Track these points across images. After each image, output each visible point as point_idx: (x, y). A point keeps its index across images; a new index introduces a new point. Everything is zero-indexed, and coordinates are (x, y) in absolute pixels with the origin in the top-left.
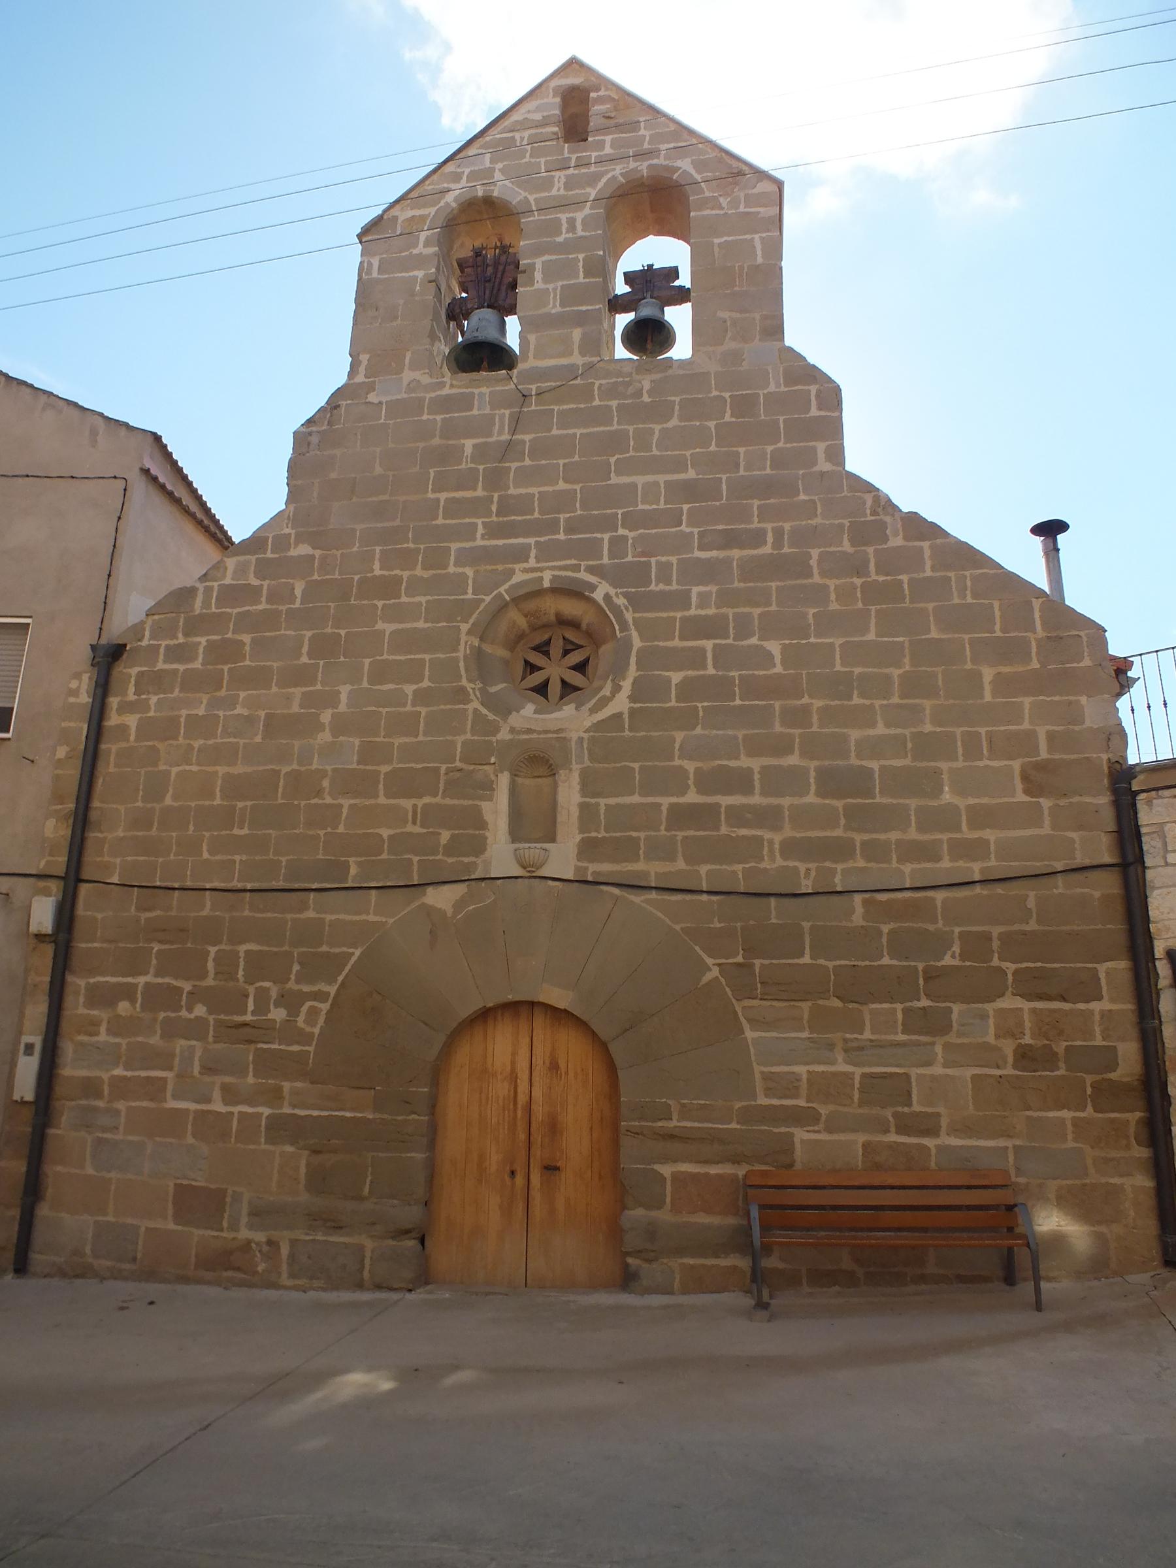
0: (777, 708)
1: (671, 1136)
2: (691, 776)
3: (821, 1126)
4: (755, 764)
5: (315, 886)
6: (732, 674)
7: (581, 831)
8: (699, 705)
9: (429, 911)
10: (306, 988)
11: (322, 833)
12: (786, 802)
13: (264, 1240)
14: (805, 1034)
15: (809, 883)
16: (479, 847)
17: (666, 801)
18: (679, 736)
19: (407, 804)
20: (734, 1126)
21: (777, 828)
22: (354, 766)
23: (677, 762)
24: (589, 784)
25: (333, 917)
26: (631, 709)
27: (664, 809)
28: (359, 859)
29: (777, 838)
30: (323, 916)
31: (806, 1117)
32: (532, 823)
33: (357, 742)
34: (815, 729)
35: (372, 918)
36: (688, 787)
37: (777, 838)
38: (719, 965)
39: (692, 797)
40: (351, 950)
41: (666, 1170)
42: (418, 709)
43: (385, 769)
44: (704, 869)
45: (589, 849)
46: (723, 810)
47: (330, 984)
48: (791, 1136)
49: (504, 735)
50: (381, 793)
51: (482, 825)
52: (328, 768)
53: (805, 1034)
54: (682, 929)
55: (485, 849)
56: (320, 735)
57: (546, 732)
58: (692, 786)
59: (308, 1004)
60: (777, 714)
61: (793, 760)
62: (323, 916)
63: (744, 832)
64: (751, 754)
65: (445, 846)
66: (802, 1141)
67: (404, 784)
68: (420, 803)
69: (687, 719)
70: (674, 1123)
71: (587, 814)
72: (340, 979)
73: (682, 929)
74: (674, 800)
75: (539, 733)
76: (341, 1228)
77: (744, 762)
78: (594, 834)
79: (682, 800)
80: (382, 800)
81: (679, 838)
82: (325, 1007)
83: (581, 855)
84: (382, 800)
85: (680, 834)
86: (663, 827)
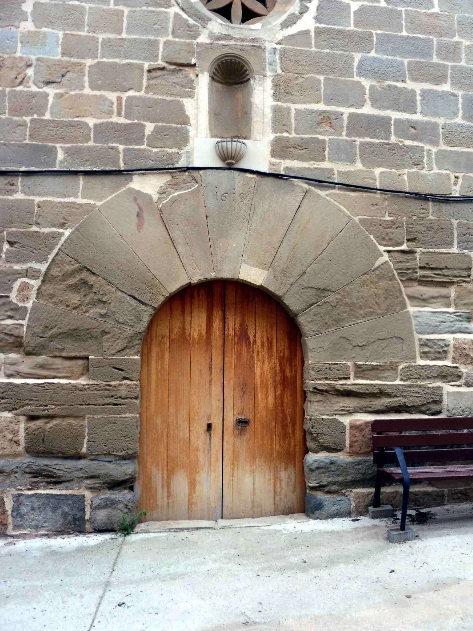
0: (435, 42)
1: (348, 394)
2: (367, 92)
3: (463, 381)
4: (417, 87)
5: (23, 169)
6: (399, 9)
7: (275, 130)
8: (374, 32)
9: (137, 195)
10: (17, 267)
11: (28, 119)
12: (441, 121)
13: (65, 233)
14: (451, 310)
15: (458, 188)
16: (182, 139)
17: (346, 111)
18: (357, 57)
19: (112, 96)
20: (398, 382)
21: (435, 143)
22: (59, 57)
23: (356, 79)
24: (281, 90)
25: (42, 199)
26: (317, 28)
27: (345, 117)
28: (67, 145)
29: (434, 150)
30: (32, 198)
31: (447, 375)
32: (232, 121)
33: (61, 34)
34: (463, 63)
35: (80, 201)
36: (365, 101)
37: (434, 150)
38: (389, 252)
39: (368, 110)
40: (61, 230)
41: (346, 420)
42: (121, 8)
43: (89, 62)
44: (377, 171)
45: (280, 149)
46: (392, 122)
47: (41, 262)
48: (440, 388)
49: (203, 39)
50: (87, 84)
51: (185, 121)
52: (33, 58)
53: (451, 310)
54: (360, 220)
55: (188, 142)
56: (23, 24)
57: (242, 40)
58: (368, 100)
59: (20, 281)
60: (435, 47)
61: (446, 87)
62: (32, 198)
63: (408, 143)
64: (414, 79)
65: (149, 136)
66: (448, 393)
67: (107, 78)
68: (125, 96)
69: (362, 42)
70: (352, 381)
71: (280, 119)
72: (51, 257)
73: (360, 220)
74: (353, 110)
75: (237, 40)
76: (61, 483)
77: (410, 85)
78: (286, 134)
79: (359, 111)
80: (87, 91)
81: (358, 143)
82: (35, 283)
83: (274, 154)
84: (87, 91)
85: (359, 140)
86: (344, 133)
